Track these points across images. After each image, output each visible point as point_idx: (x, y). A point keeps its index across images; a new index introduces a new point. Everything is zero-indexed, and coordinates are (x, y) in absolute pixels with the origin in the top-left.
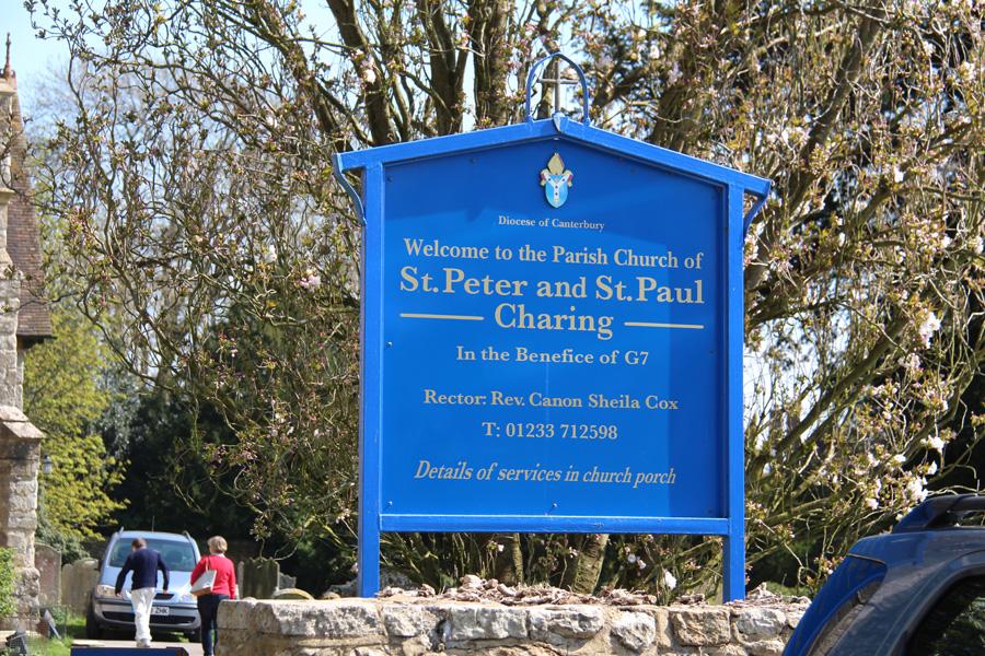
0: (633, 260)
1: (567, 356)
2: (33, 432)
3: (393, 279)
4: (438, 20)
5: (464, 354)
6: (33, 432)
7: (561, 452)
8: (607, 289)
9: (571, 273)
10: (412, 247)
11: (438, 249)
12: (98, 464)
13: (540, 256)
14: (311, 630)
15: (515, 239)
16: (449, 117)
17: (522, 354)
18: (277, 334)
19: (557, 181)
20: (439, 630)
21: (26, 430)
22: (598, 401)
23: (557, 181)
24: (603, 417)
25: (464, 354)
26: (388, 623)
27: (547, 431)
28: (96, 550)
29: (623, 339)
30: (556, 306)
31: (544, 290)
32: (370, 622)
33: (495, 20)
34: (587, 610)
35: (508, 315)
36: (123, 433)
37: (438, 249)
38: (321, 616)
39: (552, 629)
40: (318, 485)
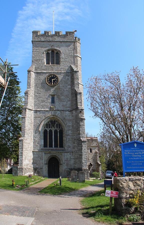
0: (142, 151)
1: (137, 158)
2: (100, 164)
3: (124, 153)
4: (126, 133)
5: (130, 159)
6: (100, 164)
7: (138, 166)
8: (140, 153)
9: (137, 152)
10: (125, 151)
11: (127, 151)
12: (105, 166)
13: (135, 151)
14: (120, 180)
15: (133, 150)
16: (128, 141)
17: (134, 158)
18: (117, 156)
19: (135, 145)
20: (129, 180)
21: (100, 163)
22: (140, 162)
23: (135, 145)
24: (141, 163)
25: (130, 159)
26: (126, 179)
27: (136, 164)
28: (106, 172)
29: (142, 157)
30: (136, 155)
31: (135, 153)
32: (124, 179)
33: (131, 132)
34: (140, 178)
35: (133, 155)
36: (107, 163)
37: (127, 151)
38: (121, 179)
39: (138, 179)
40: (121, 168)
